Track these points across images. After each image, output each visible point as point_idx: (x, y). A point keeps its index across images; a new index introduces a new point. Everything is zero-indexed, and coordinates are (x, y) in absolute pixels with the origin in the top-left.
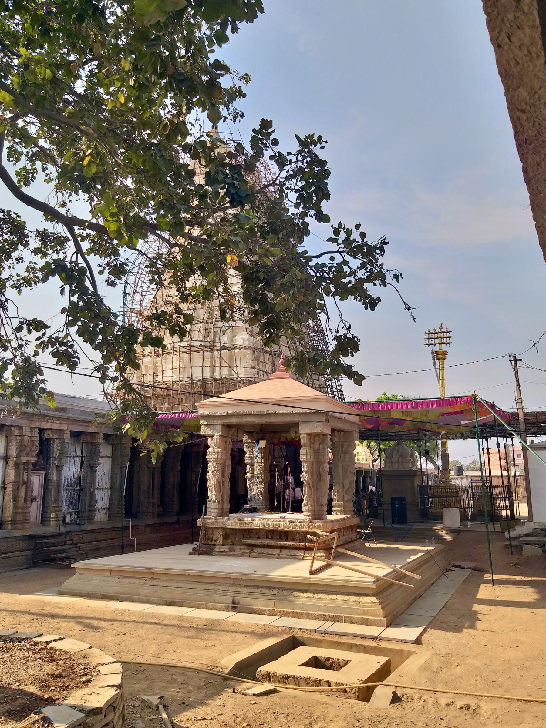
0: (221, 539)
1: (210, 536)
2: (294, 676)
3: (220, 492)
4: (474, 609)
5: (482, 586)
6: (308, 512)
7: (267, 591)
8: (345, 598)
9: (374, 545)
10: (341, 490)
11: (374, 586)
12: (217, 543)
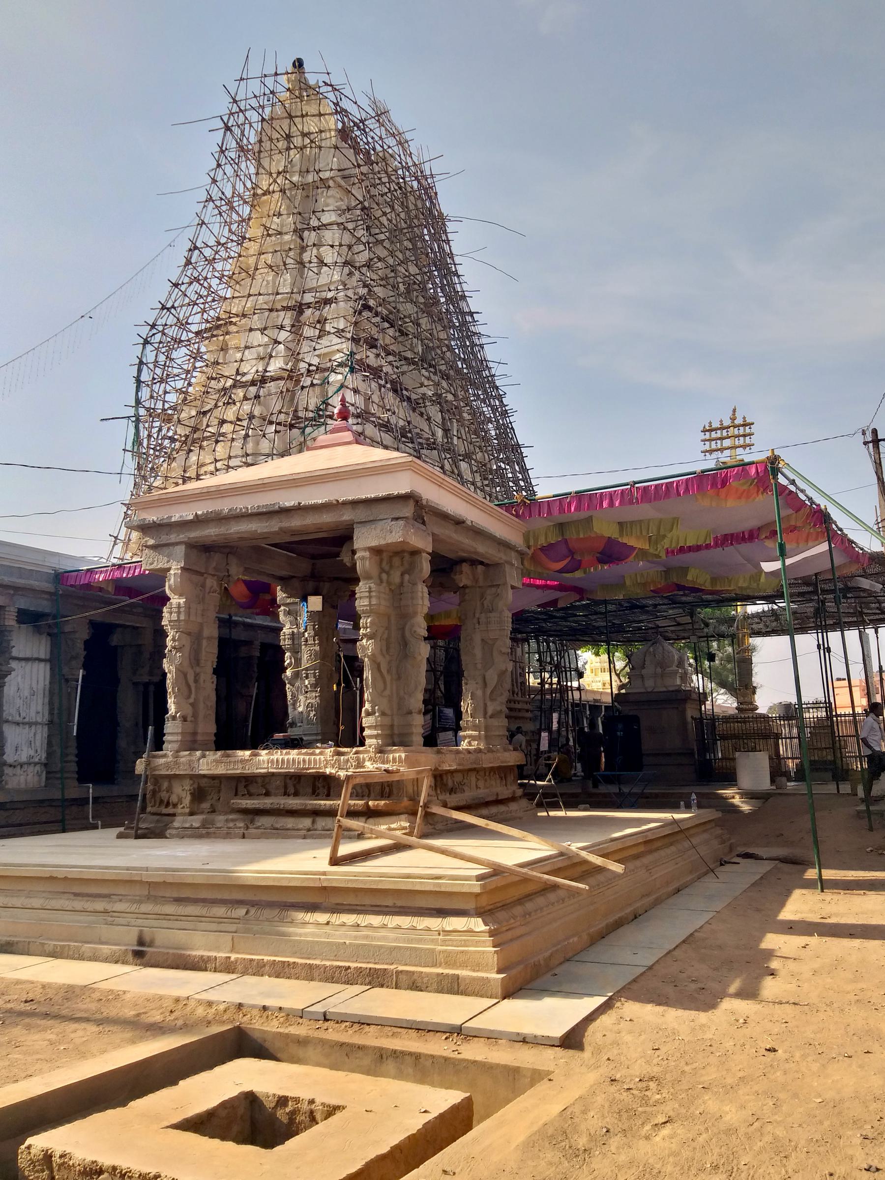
0: (187, 800)
1: (164, 795)
2: (114, 1168)
3: (189, 697)
4: (764, 945)
5: (797, 893)
6: (375, 727)
7: (220, 911)
8: (405, 921)
9: (561, 813)
10: (479, 693)
11: (476, 887)
12: (179, 810)
